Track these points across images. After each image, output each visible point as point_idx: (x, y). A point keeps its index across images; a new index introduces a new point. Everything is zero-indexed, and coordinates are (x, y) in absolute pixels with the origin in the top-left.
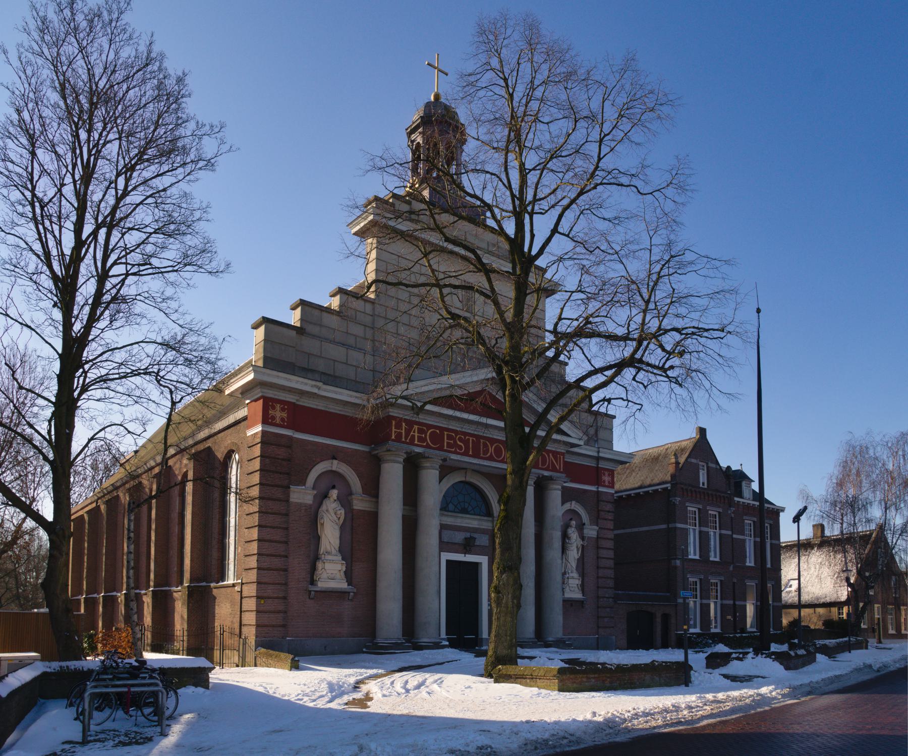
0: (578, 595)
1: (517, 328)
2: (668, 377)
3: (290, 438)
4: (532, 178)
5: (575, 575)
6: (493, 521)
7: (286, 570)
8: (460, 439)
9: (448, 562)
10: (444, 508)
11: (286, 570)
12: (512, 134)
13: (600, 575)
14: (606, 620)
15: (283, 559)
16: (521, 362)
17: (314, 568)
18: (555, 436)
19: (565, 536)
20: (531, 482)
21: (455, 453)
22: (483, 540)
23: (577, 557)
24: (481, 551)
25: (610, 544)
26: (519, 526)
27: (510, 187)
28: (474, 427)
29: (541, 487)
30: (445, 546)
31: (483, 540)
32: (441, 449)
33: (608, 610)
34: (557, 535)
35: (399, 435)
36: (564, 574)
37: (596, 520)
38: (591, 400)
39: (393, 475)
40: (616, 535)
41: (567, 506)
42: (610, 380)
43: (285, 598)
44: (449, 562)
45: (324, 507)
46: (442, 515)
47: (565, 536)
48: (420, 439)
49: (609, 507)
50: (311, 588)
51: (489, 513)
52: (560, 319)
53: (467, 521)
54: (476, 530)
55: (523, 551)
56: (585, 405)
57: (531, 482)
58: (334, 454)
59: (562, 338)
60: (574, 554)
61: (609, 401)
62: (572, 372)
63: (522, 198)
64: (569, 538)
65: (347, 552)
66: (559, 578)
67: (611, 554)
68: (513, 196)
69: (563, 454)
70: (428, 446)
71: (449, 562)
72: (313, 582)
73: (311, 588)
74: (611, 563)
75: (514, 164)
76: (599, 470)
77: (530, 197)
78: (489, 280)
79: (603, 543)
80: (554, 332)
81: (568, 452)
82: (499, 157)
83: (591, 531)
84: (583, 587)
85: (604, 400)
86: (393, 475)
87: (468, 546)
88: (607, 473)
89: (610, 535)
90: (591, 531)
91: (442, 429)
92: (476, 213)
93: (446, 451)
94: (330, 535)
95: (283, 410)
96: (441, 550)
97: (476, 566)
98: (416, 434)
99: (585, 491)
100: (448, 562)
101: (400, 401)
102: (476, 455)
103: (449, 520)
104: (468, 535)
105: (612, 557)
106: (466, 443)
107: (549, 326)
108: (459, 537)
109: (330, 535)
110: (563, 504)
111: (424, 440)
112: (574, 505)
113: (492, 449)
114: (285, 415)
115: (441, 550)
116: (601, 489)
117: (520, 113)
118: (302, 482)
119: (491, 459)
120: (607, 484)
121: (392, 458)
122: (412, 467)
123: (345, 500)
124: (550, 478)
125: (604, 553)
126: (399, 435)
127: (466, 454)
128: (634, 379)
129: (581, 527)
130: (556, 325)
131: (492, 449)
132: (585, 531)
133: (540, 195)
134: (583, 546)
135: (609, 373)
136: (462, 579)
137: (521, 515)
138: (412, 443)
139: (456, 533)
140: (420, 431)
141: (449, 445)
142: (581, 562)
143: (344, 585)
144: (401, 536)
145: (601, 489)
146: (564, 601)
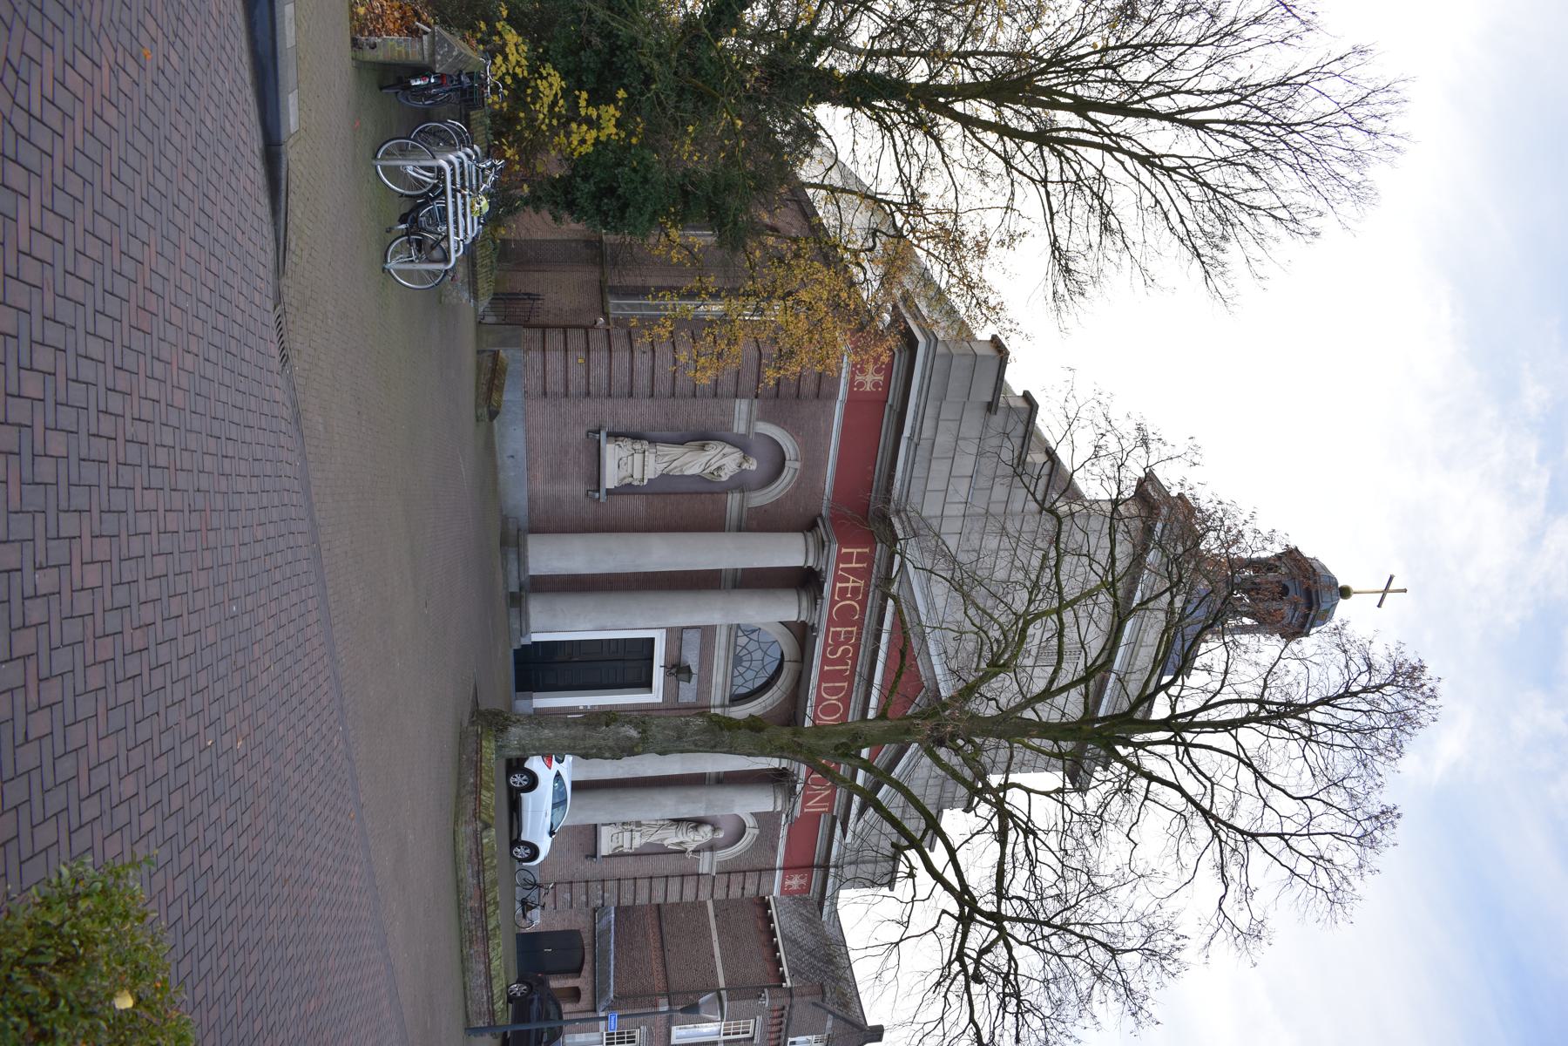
0: (605, 848)
1: (1011, 727)
2: (950, 963)
3: (833, 396)
4: (1222, 740)
5: (637, 842)
6: (723, 706)
7: (631, 395)
8: (846, 652)
9: (652, 640)
10: (735, 630)
11: (631, 395)
12: (1274, 708)
13: (639, 882)
14: (567, 896)
15: (648, 391)
16: (966, 738)
17: (636, 437)
18: (856, 798)
19: (698, 823)
20: (785, 763)
21: (826, 644)
22: (688, 693)
23: (666, 843)
24: (670, 691)
25: (689, 896)
26: (713, 748)
27: (1205, 707)
28: (865, 671)
29: (778, 779)
30: (676, 636)
31: (688, 693)
32: (831, 622)
33: (584, 898)
34: (686, 811)
35: (847, 558)
36: (639, 824)
37: (728, 871)
38: (909, 848)
39: (789, 552)
40: (704, 905)
41: (750, 822)
42: (938, 877)
43: (588, 394)
44: (650, 642)
45: (728, 449)
46: (730, 627)
47: (698, 823)
48: (843, 591)
49: (751, 890)
50: (603, 434)
51: (737, 700)
52: (1029, 791)
53: (722, 670)
54: (706, 680)
55: (677, 756)
56: (904, 842)
57: (785, 763)
58: (813, 462)
59: (996, 796)
60: (671, 838)
61: (911, 875)
62: (955, 822)
63: (1188, 727)
64: (696, 828)
65: (666, 487)
66: (632, 816)
67: (673, 898)
68: (1194, 713)
69: (831, 810)
70: (833, 603)
71: (650, 642)
72: (614, 436)
73: (603, 434)
74: (658, 898)
75: (1236, 712)
76: (817, 873)
77: (1188, 737)
78: (1073, 684)
79: (690, 885)
80: (1006, 786)
81: (834, 819)
82: (1252, 691)
83: (706, 864)
84: (617, 855)
85: (912, 868)
86: (789, 552)
87: (677, 670)
88: (803, 882)
89: (704, 895)
90: (706, 864)
91: (860, 624)
92: (1177, 658)
93: (828, 630)
94: (691, 463)
95: (876, 385)
96: (669, 630)
97: (647, 684)
98: (850, 585)
99: (774, 849)
100: (652, 640)
101: (897, 558)
102: (824, 676)
103: (721, 639)
104: (694, 670)
105: (670, 900)
106: (841, 661)
107: (1013, 778)
108: (691, 658)
109: (691, 463)
110: (754, 815)
111: (843, 598)
112: (751, 833)
113: (833, 700)
114: (868, 387)
115: (669, 630)
116: (778, 874)
117: (1314, 716)
118: (766, 417)
119: (820, 699)
120: (788, 883)
121: (811, 549)
122: (805, 581)
123: (740, 484)
124: (791, 792)
125: (674, 885)
126: (847, 558)
127: (825, 661)
128: (944, 912)
129: (712, 847)
130: (1019, 786)
131: (833, 700)
132: (707, 854)
133: (1194, 752)
134: (683, 852)
135: (950, 876)
136: (625, 663)
137: (732, 750)
138: (838, 578)
139: (697, 652)
140: (855, 591)
141: (837, 634)
142: (660, 851)
143: (611, 480)
144: (619, 571)
145: (778, 874)
146: (595, 828)
